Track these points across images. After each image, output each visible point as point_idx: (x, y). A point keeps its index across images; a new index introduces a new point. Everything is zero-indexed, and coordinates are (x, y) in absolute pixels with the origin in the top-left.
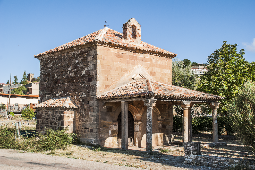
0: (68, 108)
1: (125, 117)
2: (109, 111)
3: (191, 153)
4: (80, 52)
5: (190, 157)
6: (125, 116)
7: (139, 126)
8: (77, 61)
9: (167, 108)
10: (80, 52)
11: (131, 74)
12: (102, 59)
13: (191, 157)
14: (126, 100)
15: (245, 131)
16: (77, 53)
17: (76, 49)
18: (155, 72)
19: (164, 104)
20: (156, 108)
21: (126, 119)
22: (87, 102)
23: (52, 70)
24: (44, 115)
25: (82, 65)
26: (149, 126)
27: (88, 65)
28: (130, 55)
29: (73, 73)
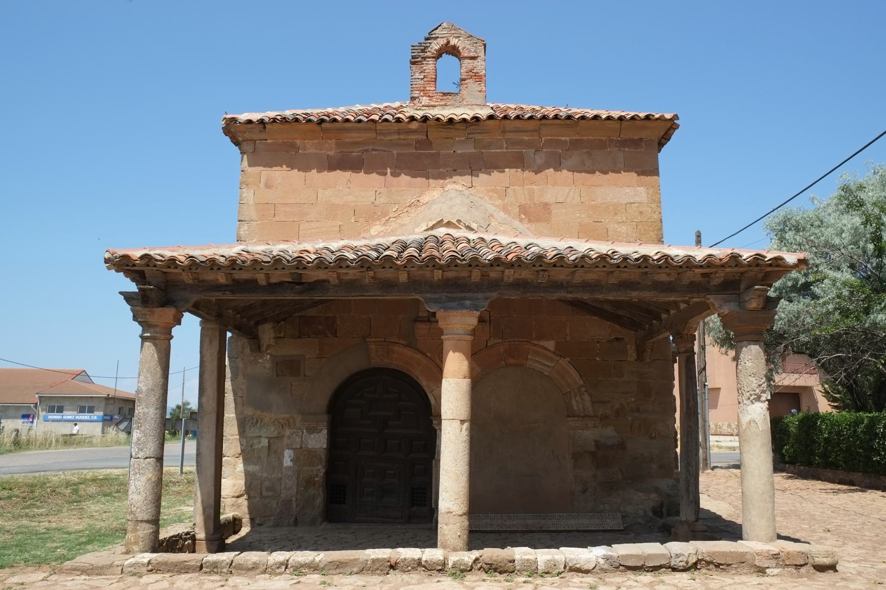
12: (262, 185)
20: (558, 358)
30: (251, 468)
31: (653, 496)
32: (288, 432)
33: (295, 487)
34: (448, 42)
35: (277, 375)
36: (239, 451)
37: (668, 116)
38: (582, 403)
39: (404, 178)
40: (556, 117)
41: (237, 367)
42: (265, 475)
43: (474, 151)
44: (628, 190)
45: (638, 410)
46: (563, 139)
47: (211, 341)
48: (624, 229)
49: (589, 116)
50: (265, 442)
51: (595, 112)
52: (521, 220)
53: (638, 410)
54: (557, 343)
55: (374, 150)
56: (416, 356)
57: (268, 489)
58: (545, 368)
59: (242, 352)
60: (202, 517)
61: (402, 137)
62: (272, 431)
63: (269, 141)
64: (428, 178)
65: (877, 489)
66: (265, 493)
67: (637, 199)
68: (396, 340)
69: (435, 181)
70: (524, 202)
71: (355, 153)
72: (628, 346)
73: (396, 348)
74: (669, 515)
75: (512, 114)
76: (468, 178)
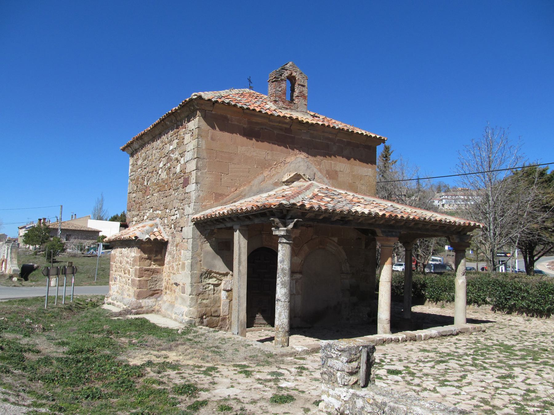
0: (144, 240)
3: (338, 379)
5: (334, 392)
7: (296, 282)
8: (171, 148)
9: (363, 247)
11: (278, 173)
12: (209, 138)
13: (339, 393)
15: (499, 273)
21: (241, 268)
22: (180, 229)
34: (292, 74)
44: (366, 169)
46: (344, 140)
48: (363, 187)
52: (327, 178)
55: (265, 129)
61: (280, 125)
63: (213, 112)
67: (369, 174)
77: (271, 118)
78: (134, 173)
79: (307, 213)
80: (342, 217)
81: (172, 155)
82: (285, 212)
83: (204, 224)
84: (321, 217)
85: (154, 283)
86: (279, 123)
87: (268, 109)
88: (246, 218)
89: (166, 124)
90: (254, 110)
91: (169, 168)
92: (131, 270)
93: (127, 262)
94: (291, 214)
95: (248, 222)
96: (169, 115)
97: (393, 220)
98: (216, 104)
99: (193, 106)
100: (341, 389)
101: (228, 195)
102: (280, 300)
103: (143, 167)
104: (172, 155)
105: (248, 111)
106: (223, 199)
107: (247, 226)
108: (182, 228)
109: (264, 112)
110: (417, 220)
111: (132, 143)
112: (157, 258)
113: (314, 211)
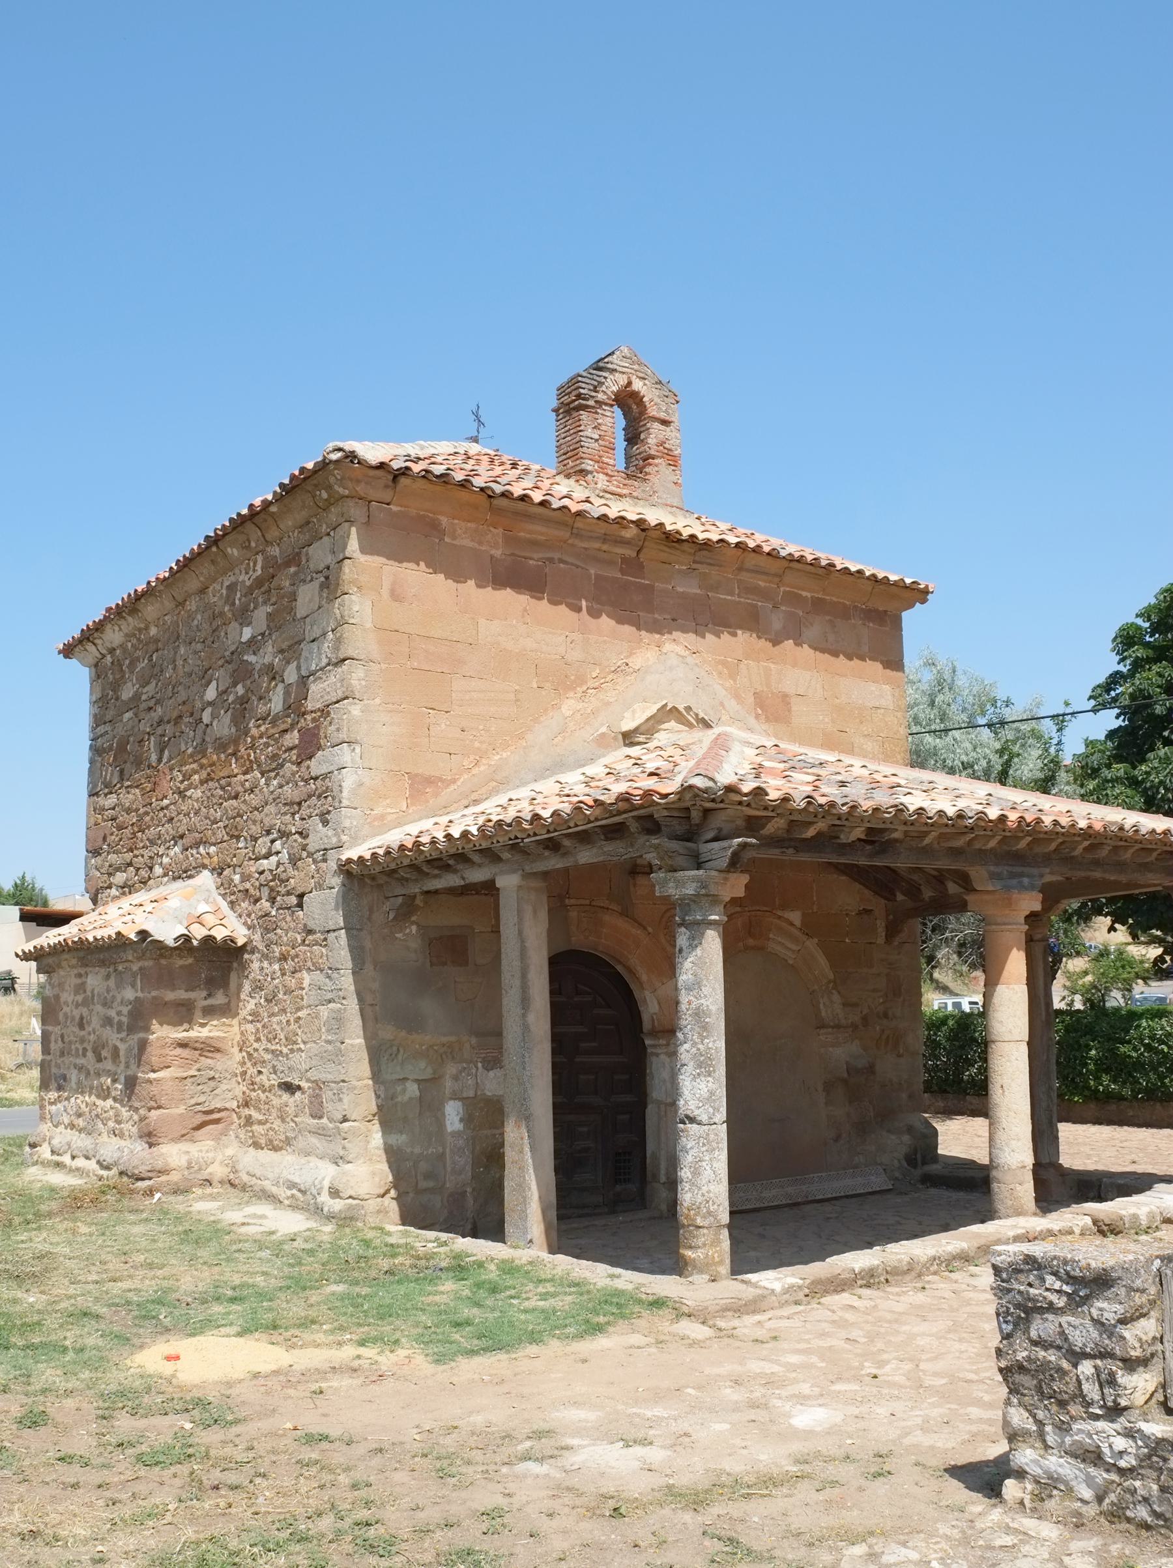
0: (170, 943)
1: (525, 1001)
2: (445, 964)
4: (259, 567)
6: (525, 988)
8: (247, 633)
9: (881, 940)
10: (259, 567)
11: (608, 704)
12: (385, 592)
14: (528, 869)
16: (244, 581)
17: (235, 552)
18: (785, 697)
19: (859, 913)
20: (804, 938)
21: (531, 1018)
23: (136, 715)
24: (70, 1000)
25: (270, 649)
26: (700, 1065)
27: (299, 642)
28: (597, 576)
29: (229, 713)
30: (400, 1139)
31: (906, 1138)
32: (451, 1069)
33: (469, 1168)
34: (630, 383)
35: (432, 965)
36: (374, 1109)
37: (320, 459)
38: (831, 1007)
39: (606, 622)
40: (465, 484)
41: (362, 948)
42: (417, 1150)
43: (698, 591)
44: (873, 687)
45: (886, 1015)
46: (804, 594)
47: (535, 912)
49: (853, 569)
50: (413, 1089)
51: (861, 567)
52: (757, 717)
53: (886, 1015)
54: (803, 915)
55: (561, 561)
56: (634, 931)
57: (428, 1176)
58: (789, 953)
59: (369, 919)
60: (542, 1226)
61: (605, 547)
62: (422, 1069)
64: (639, 629)
65: (962, 1114)
66: (423, 1184)
68: (605, 904)
69: (648, 634)
70: (760, 688)
71: (534, 559)
72: (878, 922)
73: (607, 918)
74: (924, 1163)
75: (810, 558)
76: (691, 636)
77: (579, 524)
78: (108, 727)
79: (769, 819)
80: (870, 831)
81: (251, 658)
82: (695, 815)
83: (382, 880)
84: (811, 832)
85: (206, 1088)
86: (605, 541)
87: (568, 497)
88: (547, 848)
89: (225, 555)
90: (524, 498)
91: (244, 701)
92: (122, 1047)
93: (108, 1021)
94: (718, 821)
95: (554, 863)
96: (239, 523)
97: (1029, 834)
98: (403, 481)
99: (329, 488)
100: (1101, 1425)
101: (454, 781)
102: (692, 1120)
103: (143, 706)
104: (251, 658)
105: (504, 502)
106: (436, 795)
107: (545, 875)
108: (301, 896)
109: (556, 504)
110: (1098, 833)
111: (99, 627)
112: (210, 1002)
113: (792, 812)
